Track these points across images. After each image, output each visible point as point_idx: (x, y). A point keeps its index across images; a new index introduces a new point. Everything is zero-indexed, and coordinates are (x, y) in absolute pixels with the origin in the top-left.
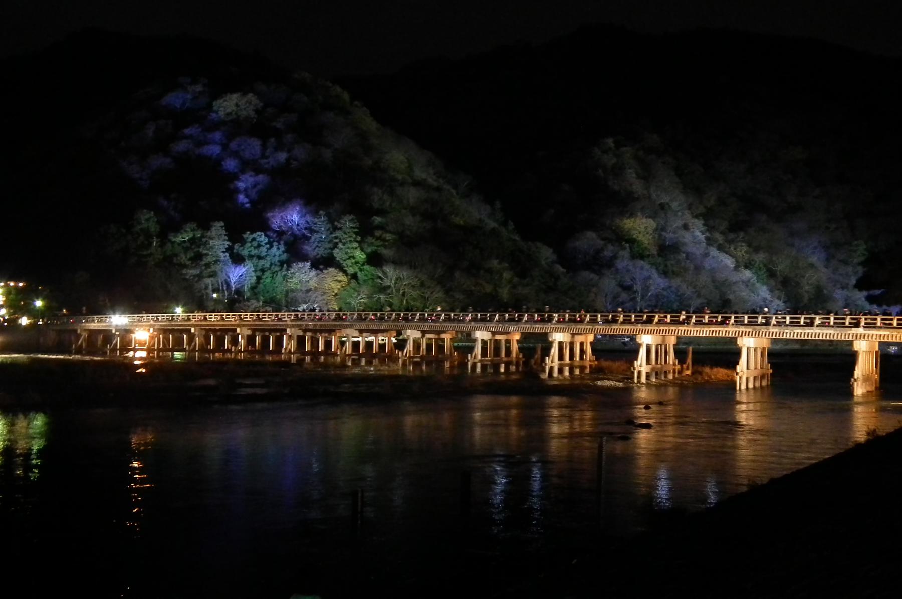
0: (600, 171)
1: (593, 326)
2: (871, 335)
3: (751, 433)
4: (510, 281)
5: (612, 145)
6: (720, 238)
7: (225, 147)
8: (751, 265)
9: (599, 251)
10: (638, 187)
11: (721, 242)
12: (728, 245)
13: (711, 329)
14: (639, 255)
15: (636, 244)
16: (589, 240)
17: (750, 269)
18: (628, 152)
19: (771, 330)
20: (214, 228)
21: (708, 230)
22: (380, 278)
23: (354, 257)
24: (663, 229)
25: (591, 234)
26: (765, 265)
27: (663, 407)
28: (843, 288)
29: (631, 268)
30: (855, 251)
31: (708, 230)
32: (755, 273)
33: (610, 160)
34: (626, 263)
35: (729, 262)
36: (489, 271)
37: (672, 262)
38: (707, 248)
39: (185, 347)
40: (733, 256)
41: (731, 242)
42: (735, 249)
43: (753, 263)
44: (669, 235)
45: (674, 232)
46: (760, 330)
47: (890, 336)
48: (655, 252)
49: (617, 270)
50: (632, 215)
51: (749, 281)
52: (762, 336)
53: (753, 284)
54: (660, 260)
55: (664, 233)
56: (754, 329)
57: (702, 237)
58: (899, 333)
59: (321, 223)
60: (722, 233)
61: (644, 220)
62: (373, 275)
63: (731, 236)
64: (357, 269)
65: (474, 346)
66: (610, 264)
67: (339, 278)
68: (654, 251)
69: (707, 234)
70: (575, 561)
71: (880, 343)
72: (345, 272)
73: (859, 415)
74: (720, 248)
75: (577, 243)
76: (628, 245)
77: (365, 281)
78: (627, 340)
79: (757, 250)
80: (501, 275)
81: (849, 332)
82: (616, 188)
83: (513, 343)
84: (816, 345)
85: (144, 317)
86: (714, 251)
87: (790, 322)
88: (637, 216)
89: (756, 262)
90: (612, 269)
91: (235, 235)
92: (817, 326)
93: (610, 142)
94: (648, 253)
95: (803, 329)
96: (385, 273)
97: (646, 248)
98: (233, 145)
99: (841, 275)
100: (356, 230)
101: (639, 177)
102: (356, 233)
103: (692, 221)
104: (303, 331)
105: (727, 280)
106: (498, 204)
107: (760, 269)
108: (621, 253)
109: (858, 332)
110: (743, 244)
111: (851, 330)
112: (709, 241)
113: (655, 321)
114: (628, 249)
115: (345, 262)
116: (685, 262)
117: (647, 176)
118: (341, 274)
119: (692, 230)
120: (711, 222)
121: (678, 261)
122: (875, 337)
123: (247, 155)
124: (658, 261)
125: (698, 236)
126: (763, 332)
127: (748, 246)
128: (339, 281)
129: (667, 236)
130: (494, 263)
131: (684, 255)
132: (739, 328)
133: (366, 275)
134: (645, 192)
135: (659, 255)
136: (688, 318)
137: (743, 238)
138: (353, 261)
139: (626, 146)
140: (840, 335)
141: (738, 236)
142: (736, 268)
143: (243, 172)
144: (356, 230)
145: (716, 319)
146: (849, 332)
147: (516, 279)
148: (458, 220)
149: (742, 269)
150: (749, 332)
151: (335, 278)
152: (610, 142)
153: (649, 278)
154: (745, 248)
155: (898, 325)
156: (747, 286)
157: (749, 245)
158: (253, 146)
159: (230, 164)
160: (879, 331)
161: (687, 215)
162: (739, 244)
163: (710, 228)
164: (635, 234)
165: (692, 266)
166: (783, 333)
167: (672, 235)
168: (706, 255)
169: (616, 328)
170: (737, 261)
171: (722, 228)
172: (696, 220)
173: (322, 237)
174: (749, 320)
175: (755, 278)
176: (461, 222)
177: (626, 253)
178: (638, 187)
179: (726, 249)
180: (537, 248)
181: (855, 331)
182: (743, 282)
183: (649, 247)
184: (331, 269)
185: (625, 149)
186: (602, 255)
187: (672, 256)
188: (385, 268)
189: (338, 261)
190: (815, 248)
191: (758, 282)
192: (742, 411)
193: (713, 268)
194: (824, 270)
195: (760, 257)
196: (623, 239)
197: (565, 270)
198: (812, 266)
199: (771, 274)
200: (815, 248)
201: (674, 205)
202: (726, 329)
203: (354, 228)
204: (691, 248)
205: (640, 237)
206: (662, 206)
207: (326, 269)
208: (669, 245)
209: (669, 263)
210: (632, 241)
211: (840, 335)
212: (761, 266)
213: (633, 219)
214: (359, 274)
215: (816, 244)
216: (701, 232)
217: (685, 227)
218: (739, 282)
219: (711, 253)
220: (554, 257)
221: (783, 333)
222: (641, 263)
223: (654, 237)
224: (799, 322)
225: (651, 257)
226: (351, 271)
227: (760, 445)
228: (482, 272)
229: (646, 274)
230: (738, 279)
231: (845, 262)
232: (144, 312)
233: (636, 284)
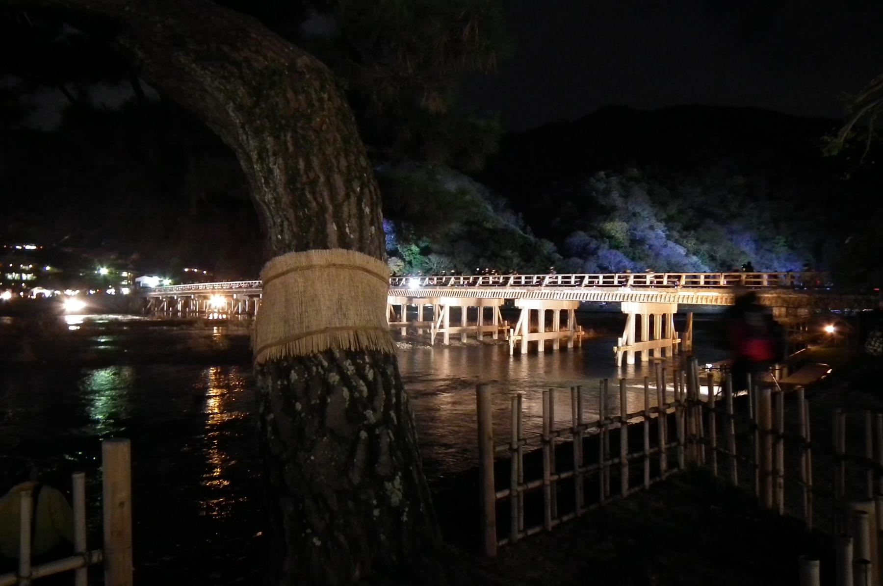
0: (594, 193)
1: (453, 289)
2: (638, 296)
4: (518, 265)
5: (604, 176)
6: (676, 235)
8: (698, 253)
9: (588, 244)
10: (619, 202)
11: (677, 238)
12: (682, 240)
13: (493, 291)
14: (615, 246)
15: (614, 240)
16: (580, 237)
17: (697, 256)
18: (614, 180)
19: (544, 291)
21: (668, 230)
22: (427, 263)
23: (411, 250)
24: (635, 229)
25: (581, 233)
26: (709, 254)
27: (476, 375)
28: (767, 268)
29: (608, 255)
30: (778, 243)
31: (668, 230)
32: (701, 257)
33: (602, 186)
34: (605, 252)
35: (682, 251)
36: (505, 258)
37: (639, 251)
38: (666, 242)
39: (192, 308)
40: (684, 247)
41: (684, 237)
42: (687, 242)
43: (699, 251)
44: (639, 234)
45: (643, 231)
46: (534, 290)
47: (658, 296)
48: (628, 245)
49: (599, 256)
50: (612, 220)
51: (696, 263)
52: (535, 297)
53: (699, 266)
54: (630, 250)
55: (635, 232)
56: (528, 290)
57: (663, 235)
58: (668, 293)
60: (678, 232)
61: (620, 223)
62: (422, 261)
63: (685, 233)
64: (412, 258)
66: (594, 252)
67: (398, 264)
68: (627, 243)
69: (668, 233)
71: (505, 299)
72: (404, 260)
73: (630, 400)
74: (677, 242)
75: (572, 240)
76: (608, 240)
77: (416, 265)
78: (604, 303)
79: (703, 242)
80: (512, 261)
81: (616, 292)
82: (603, 203)
84: (601, 306)
85: (245, 288)
86: (671, 244)
87: (604, 282)
88: (615, 221)
89: (701, 250)
90: (595, 256)
92: (547, 286)
94: (622, 245)
95: (572, 289)
96: (429, 259)
97: (621, 242)
99: (767, 259)
101: (620, 196)
103: (657, 223)
104: (249, 297)
105: (679, 263)
107: (704, 255)
108: (602, 245)
109: (625, 293)
110: (693, 239)
111: (618, 290)
112: (669, 237)
113: (450, 283)
114: (608, 242)
115: (404, 254)
116: (648, 251)
117: (627, 195)
118: (400, 261)
119: (656, 230)
120: (670, 224)
121: (643, 251)
122: (642, 298)
124: (629, 251)
125: (660, 234)
126: (536, 293)
127: (696, 240)
128: (399, 266)
129: (637, 233)
130: (509, 252)
131: (647, 246)
132: (515, 289)
133: (417, 261)
134: (624, 206)
135: (630, 246)
136: (507, 280)
137: (693, 235)
138: (410, 252)
140: (607, 295)
141: (690, 234)
142: (687, 255)
145: (468, 281)
146: (616, 292)
147: (522, 263)
148: (489, 225)
149: (691, 255)
150: (525, 293)
151: (396, 264)
152: (602, 174)
153: (620, 262)
154: (694, 241)
155: (646, 276)
156: (694, 267)
157: (697, 239)
160: (647, 290)
161: (653, 221)
162: (690, 239)
163: (670, 229)
164: (613, 233)
165: (653, 254)
166: (554, 293)
167: (640, 233)
168: (666, 246)
169: (473, 290)
170: (688, 250)
171: (678, 228)
172: (659, 223)
173: (391, 238)
174: (526, 280)
175: (700, 261)
176: (491, 227)
177: (606, 246)
178: (619, 202)
179: (681, 243)
180: (542, 242)
181: (622, 290)
182: (691, 264)
183: (623, 241)
184: (393, 258)
186: (588, 247)
187: (639, 247)
188: (430, 257)
189: (400, 253)
190: (748, 241)
191: (702, 264)
193: (668, 255)
194: (754, 256)
195: (705, 247)
196: (604, 236)
197: (562, 257)
198: (743, 253)
199: (713, 258)
200: (748, 241)
201: (645, 214)
202: (505, 291)
204: (656, 243)
205: (618, 235)
206: (634, 214)
207: (391, 258)
208: (638, 240)
209: (636, 252)
210: (611, 238)
211: (607, 295)
212: (705, 253)
213: (612, 223)
215: (748, 238)
216: (662, 231)
217: (652, 228)
218: (688, 264)
219: (669, 245)
220: (555, 248)
221: (554, 293)
222: (614, 251)
223: (627, 235)
224: (613, 282)
225: (623, 248)
226: (407, 259)
227: (526, 427)
228: (499, 258)
229: (618, 259)
230: (687, 262)
231: (770, 251)
232: (182, 283)
233: (611, 266)
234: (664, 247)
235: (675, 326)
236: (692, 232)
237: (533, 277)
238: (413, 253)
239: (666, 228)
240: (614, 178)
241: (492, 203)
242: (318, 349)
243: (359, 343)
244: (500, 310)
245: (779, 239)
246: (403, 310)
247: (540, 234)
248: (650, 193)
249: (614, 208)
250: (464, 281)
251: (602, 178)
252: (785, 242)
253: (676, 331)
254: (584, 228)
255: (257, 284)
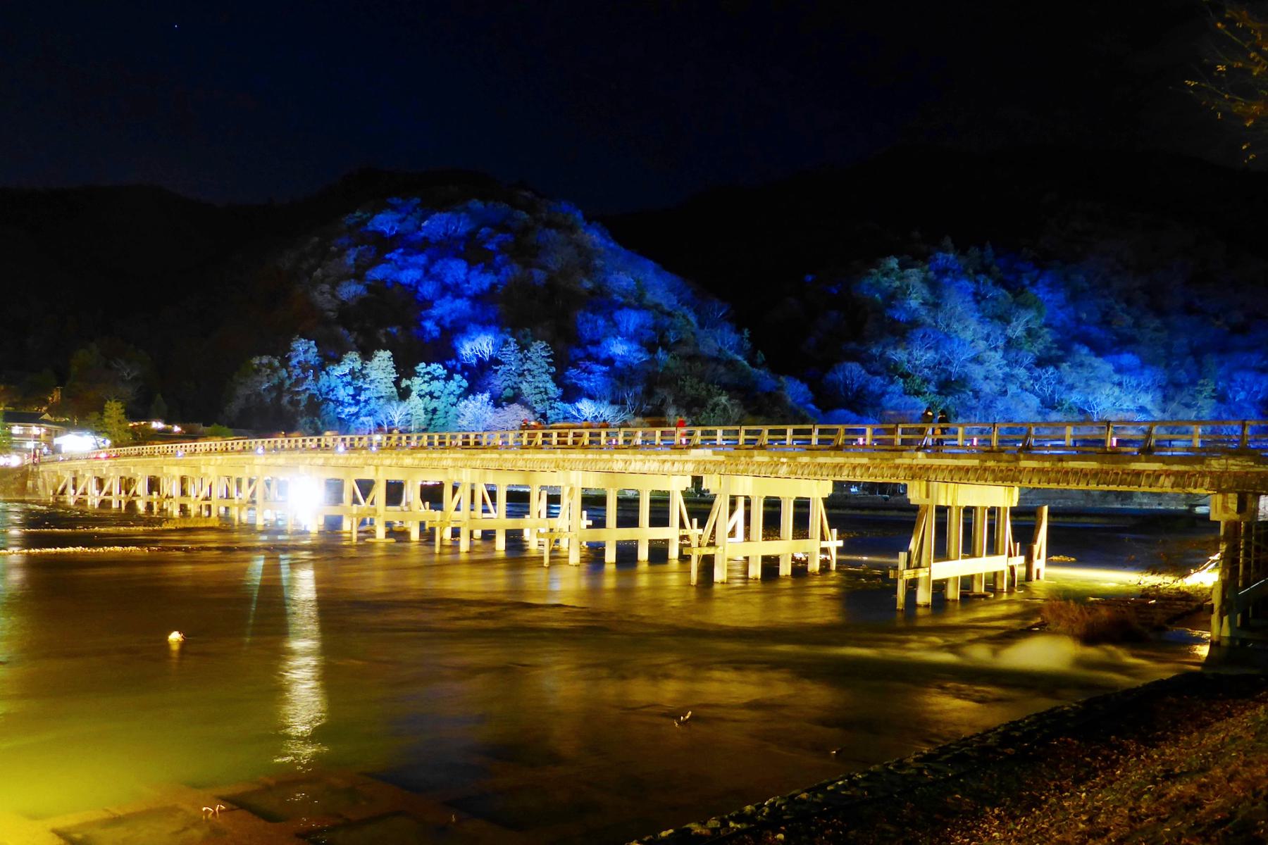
3: (70, 519)
7: (426, 272)
20: (376, 359)
24: (948, 362)
30: (1201, 392)
31: (1007, 365)
59: (511, 355)
65: (710, 510)
70: (664, 834)
83: (975, 533)
91: (404, 368)
93: (893, 263)
98: (437, 268)
100: (550, 360)
102: (550, 364)
106: (746, 333)
123: (449, 280)
139: (912, 267)
143: (442, 296)
144: (550, 360)
152: (893, 263)
158: (456, 270)
159: (428, 289)
185: (910, 270)
188: (579, 405)
192: (737, 571)
196: (892, 371)
203: (548, 357)
214: (549, 413)
226: (539, 407)
234: (1000, 395)
235: (1013, 534)
236: (1051, 369)
237: (567, 433)
238: (548, 399)
239: (1005, 362)
240: (915, 270)
241: (697, 312)
242: (757, 592)
243: (302, 563)
244: (686, 502)
245: (1203, 385)
246: (518, 506)
247: (778, 366)
248: (978, 298)
249: (914, 324)
250: (400, 435)
251: (893, 270)
252: (1214, 391)
253: (1015, 541)
254: (854, 357)
255: (137, 452)
